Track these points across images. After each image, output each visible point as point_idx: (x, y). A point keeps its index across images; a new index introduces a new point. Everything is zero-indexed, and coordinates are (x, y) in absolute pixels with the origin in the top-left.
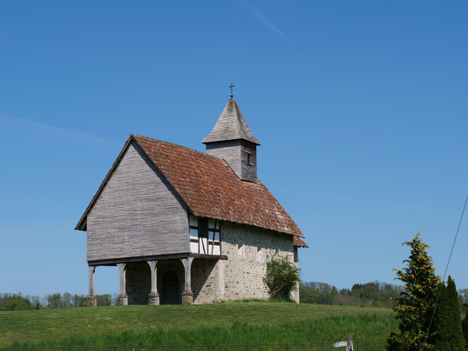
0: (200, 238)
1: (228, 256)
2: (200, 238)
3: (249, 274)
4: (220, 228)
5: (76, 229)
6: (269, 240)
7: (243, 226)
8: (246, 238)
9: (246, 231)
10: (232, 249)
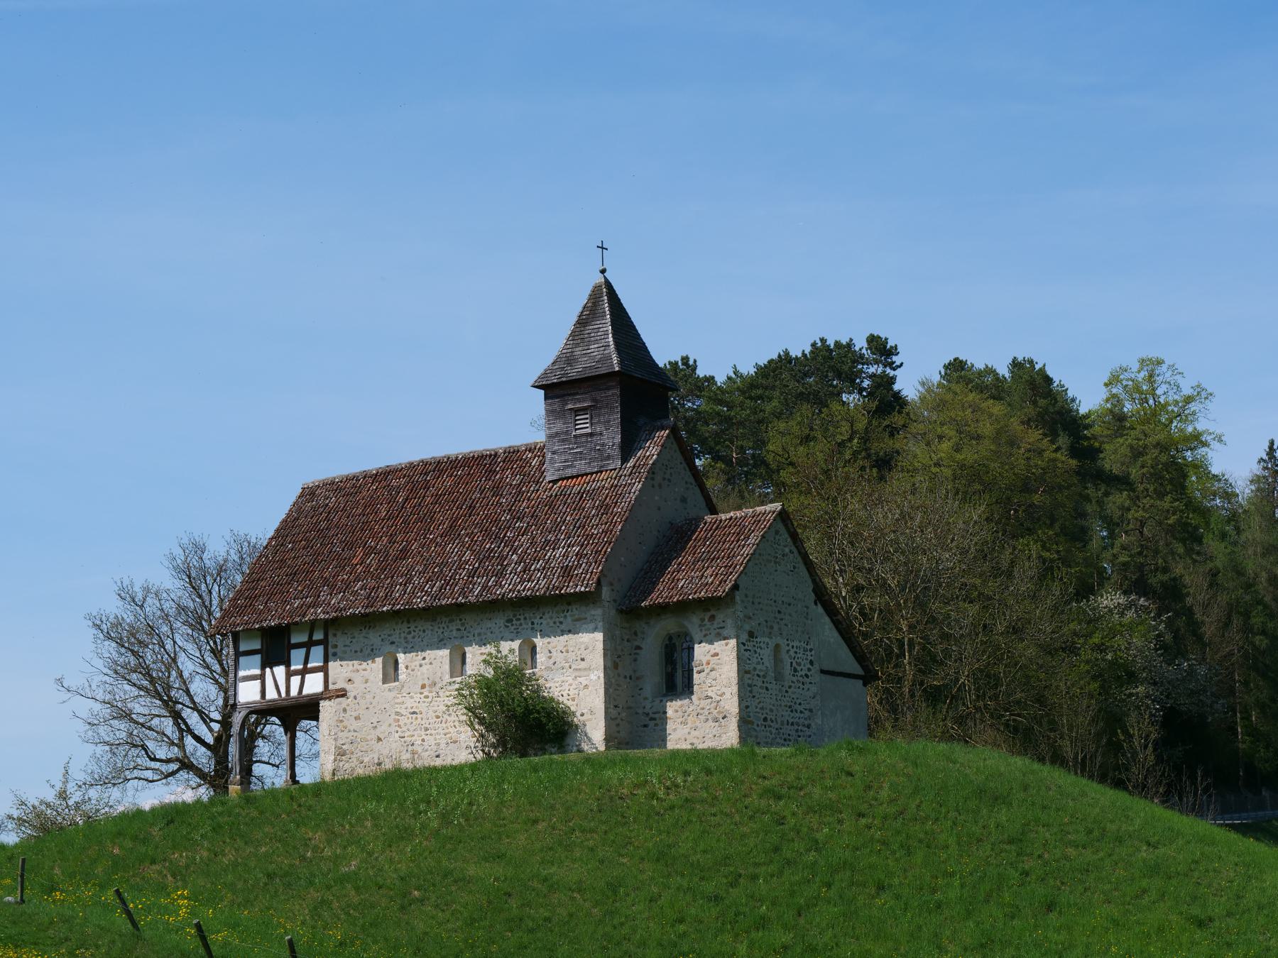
0: (268, 670)
1: (348, 687)
2: (268, 670)
3: (419, 716)
4: (326, 635)
5: (851, 340)
6: (499, 621)
7: (396, 615)
8: (409, 637)
9: (409, 622)
10: (365, 670)
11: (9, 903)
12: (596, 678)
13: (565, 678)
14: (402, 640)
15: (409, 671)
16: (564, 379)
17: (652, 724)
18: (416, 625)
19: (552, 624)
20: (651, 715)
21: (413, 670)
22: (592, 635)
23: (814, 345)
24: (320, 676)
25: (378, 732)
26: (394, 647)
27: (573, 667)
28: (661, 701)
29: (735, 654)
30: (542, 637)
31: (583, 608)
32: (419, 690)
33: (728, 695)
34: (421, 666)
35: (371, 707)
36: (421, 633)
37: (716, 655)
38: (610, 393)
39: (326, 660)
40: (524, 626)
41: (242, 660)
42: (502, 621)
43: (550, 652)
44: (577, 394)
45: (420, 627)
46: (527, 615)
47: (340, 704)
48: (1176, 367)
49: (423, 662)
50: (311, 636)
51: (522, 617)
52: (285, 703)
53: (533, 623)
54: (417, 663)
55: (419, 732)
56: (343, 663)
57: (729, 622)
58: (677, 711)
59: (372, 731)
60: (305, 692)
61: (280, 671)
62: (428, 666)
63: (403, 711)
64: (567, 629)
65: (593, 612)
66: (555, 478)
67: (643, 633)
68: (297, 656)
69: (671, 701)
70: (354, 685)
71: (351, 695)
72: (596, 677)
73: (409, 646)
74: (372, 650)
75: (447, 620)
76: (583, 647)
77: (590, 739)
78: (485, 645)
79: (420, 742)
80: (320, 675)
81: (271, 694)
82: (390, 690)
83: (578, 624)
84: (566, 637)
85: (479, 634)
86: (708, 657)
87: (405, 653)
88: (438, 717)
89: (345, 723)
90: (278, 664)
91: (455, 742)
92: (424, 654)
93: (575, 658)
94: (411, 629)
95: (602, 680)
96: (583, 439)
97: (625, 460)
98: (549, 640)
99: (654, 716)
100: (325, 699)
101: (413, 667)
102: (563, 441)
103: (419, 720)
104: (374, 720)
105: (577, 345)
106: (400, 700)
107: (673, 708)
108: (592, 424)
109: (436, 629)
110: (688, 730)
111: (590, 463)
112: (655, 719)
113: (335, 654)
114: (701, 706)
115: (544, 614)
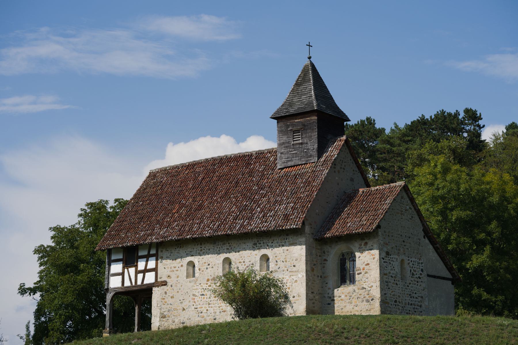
1: (168, 280)
2: (126, 270)
3: (205, 296)
15: (201, 271)
16: (287, 114)
21: (203, 271)
25: (183, 305)
32: (206, 282)
33: (374, 287)
34: (207, 269)
43: (277, 262)
46: (264, 241)
47: (163, 289)
49: (208, 267)
50: (149, 252)
51: (262, 242)
52: (135, 289)
60: (145, 282)
62: (211, 269)
63: (197, 294)
65: (300, 240)
66: (282, 167)
67: (328, 252)
71: (169, 284)
76: (294, 259)
79: (205, 311)
81: (127, 284)
82: (190, 282)
91: (224, 311)
94: (202, 248)
101: (203, 269)
106: (196, 287)
108: (302, 138)
109: (216, 249)
110: (352, 307)
111: (301, 159)
115: (274, 240)
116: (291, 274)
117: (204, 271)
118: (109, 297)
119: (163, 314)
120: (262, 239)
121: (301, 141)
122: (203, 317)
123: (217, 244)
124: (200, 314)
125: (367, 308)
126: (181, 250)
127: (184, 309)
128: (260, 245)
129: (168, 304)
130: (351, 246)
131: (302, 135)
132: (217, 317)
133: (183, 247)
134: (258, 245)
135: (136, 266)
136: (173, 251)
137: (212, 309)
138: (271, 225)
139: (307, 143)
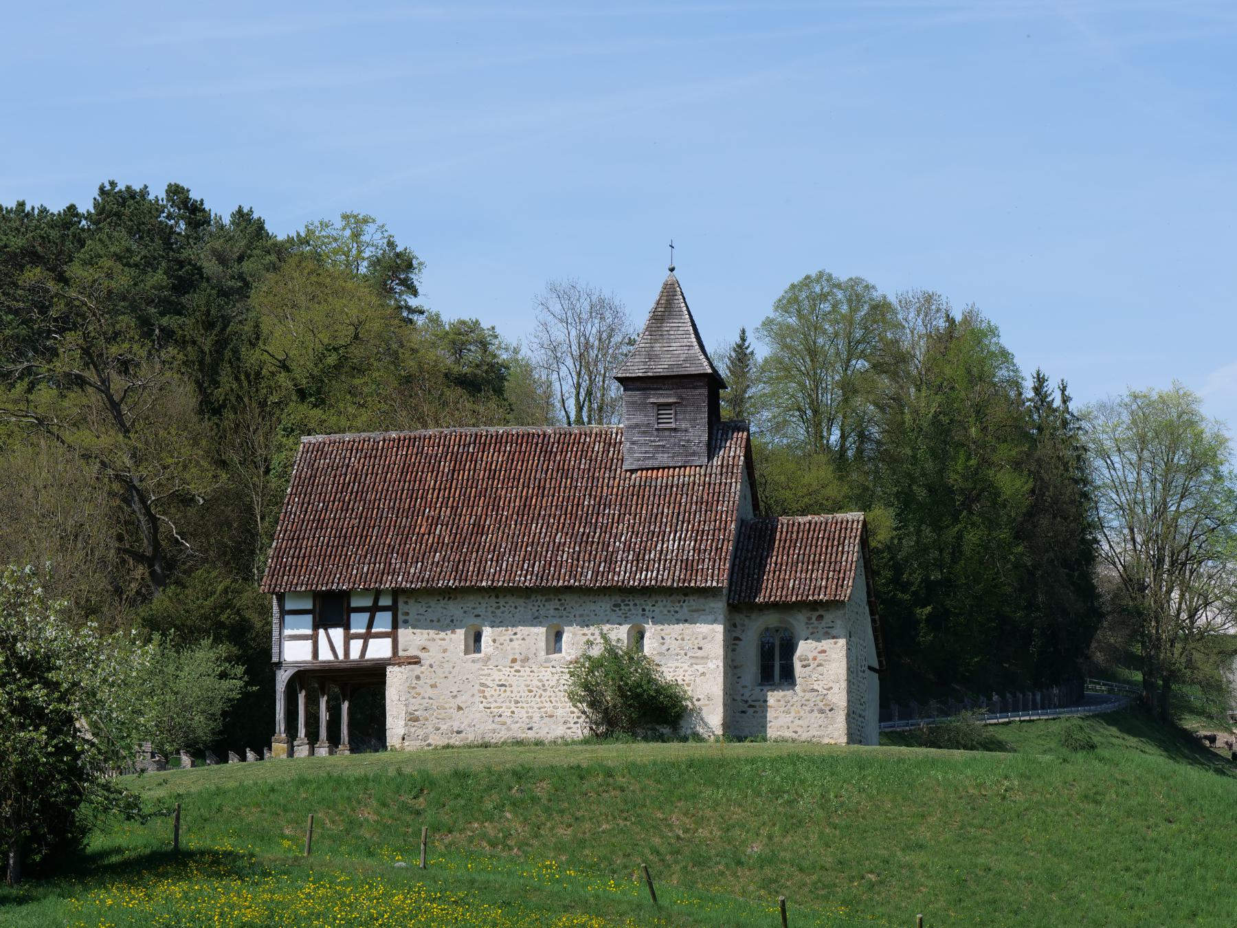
0: (321, 632)
1: (422, 655)
2: (321, 632)
3: (508, 689)
5: (146, 187)
6: (605, 605)
7: (493, 591)
8: (498, 612)
10: (444, 640)
11: (401, 868)
12: (715, 666)
13: (679, 665)
14: (489, 614)
15: (497, 644)
16: (650, 374)
17: (751, 711)
18: (506, 600)
19: (666, 612)
20: (750, 703)
21: (502, 644)
22: (710, 627)
23: (102, 189)
24: (388, 642)
25: (459, 701)
26: (478, 621)
27: (690, 654)
28: (762, 690)
29: (844, 652)
30: (654, 623)
31: (702, 600)
32: (509, 663)
33: (835, 690)
34: (511, 640)
35: (450, 676)
36: (511, 609)
37: (824, 652)
38: (698, 392)
39: (395, 626)
40: (633, 612)
41: (287, 618)
42: (608, 605)
43: (663, 638)
44: (661, 389)
45: (510, 603)
46: (637, 602)
47: (412, 670)
48: (385, 228)
49: (514, 637)
50: (376, 601)
51: (631, 603)
52: (344, 665)
53: (644, 610)
54: (508, 638)
55: (508, 704)
56: (415, 631)
57: (839, 623)
58: (779, 701)
59: (451, 700)
60: (368, 656)
61: (337, 634)
62: (521, 642)
63: (489, 683)
64: (683, 618)
65: (712, 605)
66: (634, 467)
67: (743, 625)
68: (358, 624)
69: (773, 690)
70: (430, 654)
71: (426, 662)
72: (715, 666)
73: (498, 621)
74: (452, 621)
75: (544, 599)
76: (701, 636)
77: (706, 724)
78: (587, 626)
79: (509, 714)
80: (388, 641)
81: (325, 655)
82: (473, 661)
83: (696, 615)
84: (681, 626)
85: (581, 616)
86: (815, 654)
87: (492, 627)
88: (530, 691)
89: (418, 690)
90: (335, 626)
91: (551, 716)
92: (515, 630)
93: (691, 647)
94: (501, 604)
95: (721, 669)
96: (667, 433)
97: (710, 458)
98: (662, 627)
99: (753, 703)
100: (394, 665)
101: (502, 641)
102: (644, 432)
103: (508, 693)
104: (455, 689)
105: (656, 341)
106: (486, 672)
107: (774, 698)
108: (676, 420)
109: (530, 607)
110: (791, 719)
111: (673, 457)
112: (754, 707)
113: (406, 622)
114: (806, 698)
115: (657, 602)
116: (693, 661)
117: (505, 644)
118: (282, 678)
119: (411, 714)
120: (631, 598)
121: (673, 426)
122: (504, 724)
123: (533, 598)
124: (497, 719)
125: (820, 723)
126: (451, 602)
127: (460, 708)
128: (627, 608)
129: (424, 698)
130: (791, 620)
131: (676, 414)
132: (536, 726)
133: (456, 598)
134: (623, 607)
135: (347, 627)
136: (432, 604)
137: (523, 711)
138: (648, 577)
139: (686, 431)
